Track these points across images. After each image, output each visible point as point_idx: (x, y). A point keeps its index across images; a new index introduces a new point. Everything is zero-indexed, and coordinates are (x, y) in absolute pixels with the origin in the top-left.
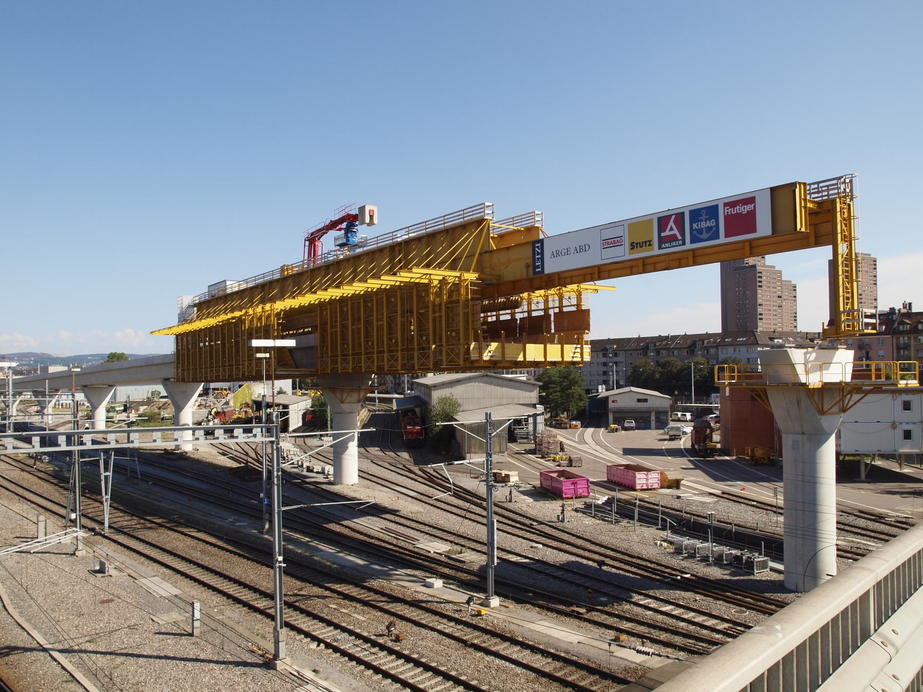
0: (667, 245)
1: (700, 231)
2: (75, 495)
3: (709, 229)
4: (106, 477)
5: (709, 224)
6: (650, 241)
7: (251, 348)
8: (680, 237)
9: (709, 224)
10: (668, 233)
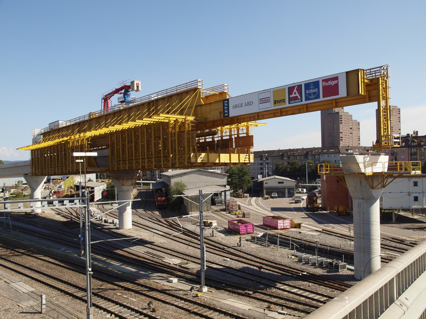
3: (314, 93)
5: (314, 91)
6: (284, 100)
8: (299, 98)
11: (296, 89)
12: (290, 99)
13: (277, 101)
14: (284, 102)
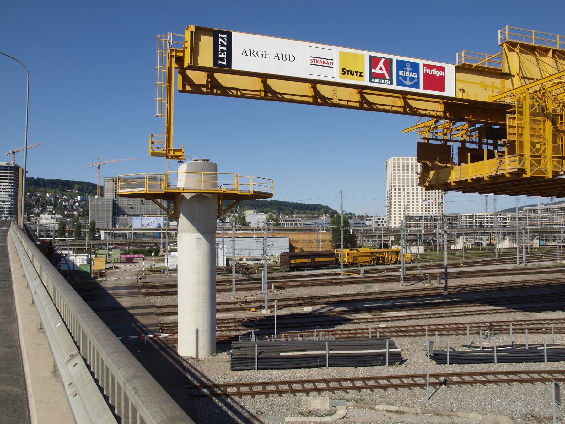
0: (377, 80)
1: (405, 78)
2: (321, 331)
3: (412, 79)
4: (366, 272)
5: (412, 75)
6: (361, 73)
7: (461, 50)
8: (388, 78)
9: (412, 75)
10: (377, 71)
11: (384, 74)
12: (372, 76)
13: (348, 71)
14: (360, 76)
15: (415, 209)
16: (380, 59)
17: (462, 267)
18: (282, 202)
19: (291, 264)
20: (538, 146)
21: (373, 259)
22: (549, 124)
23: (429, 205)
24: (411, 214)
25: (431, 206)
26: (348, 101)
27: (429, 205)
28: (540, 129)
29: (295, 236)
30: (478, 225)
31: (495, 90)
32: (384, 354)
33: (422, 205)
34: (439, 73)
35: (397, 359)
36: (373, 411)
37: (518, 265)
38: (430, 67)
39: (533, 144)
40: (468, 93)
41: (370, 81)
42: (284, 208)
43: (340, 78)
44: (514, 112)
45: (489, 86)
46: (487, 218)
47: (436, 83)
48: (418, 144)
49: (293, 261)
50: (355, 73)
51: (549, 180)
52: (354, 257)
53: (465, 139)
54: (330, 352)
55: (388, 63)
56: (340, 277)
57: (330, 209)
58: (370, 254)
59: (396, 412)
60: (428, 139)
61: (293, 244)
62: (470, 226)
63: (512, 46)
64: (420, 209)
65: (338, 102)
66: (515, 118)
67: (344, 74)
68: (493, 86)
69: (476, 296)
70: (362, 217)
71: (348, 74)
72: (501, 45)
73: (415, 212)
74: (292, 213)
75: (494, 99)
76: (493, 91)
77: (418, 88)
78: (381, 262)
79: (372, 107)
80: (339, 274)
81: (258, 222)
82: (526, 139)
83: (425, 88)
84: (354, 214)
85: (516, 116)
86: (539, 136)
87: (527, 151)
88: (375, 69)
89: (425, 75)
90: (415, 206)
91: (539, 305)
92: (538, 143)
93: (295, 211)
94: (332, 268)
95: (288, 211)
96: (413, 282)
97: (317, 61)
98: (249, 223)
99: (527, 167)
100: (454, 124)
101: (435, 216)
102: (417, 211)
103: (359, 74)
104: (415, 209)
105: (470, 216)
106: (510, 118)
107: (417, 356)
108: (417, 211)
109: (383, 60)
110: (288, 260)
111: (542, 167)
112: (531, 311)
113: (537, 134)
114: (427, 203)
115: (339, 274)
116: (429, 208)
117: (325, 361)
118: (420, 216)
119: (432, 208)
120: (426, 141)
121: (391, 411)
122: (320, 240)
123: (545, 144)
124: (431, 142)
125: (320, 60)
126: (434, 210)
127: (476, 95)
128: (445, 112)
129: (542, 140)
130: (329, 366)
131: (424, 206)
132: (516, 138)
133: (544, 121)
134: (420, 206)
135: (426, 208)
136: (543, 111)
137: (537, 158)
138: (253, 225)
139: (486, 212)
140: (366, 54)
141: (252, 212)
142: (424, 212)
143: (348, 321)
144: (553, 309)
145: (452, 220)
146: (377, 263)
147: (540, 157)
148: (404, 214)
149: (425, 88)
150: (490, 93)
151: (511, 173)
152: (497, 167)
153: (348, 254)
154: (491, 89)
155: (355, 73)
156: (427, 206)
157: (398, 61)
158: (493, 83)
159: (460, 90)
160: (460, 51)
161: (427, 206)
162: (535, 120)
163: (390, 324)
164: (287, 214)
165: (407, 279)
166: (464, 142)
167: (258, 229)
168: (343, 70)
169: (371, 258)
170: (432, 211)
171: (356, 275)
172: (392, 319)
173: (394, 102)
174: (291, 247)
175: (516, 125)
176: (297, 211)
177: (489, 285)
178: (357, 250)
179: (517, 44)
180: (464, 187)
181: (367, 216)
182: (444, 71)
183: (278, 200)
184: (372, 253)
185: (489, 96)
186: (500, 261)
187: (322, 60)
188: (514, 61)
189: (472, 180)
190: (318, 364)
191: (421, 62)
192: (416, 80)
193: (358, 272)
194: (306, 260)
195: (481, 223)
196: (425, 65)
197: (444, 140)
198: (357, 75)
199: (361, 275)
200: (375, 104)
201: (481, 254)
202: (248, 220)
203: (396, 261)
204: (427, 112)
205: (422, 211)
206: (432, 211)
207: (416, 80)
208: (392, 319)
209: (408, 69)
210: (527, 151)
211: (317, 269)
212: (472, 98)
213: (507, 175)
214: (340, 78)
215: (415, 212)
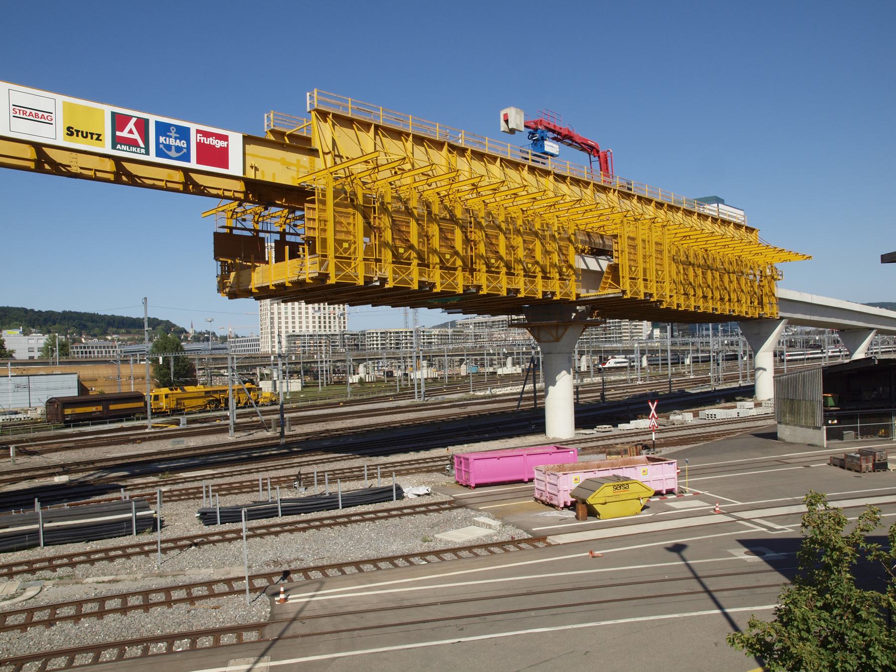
1: (169, 147)
3: (178, 149)
4: (190, 422)
6: (99, 135)
8: (142, 145)
9: (178, 143)
10: (125, 134)
11: (136, 140)
12: (116, 141)
13: (78, 131)
14: (98, 139)
15: (304, 325)
16: (129, 118)
17: (342, 406)
18: (85, 314)
19: (65, 416)
20: (346, 245)
21: (210, 402)
22: (360, 219)
23: (325, 318)
24: (297, 332)
25: (327, 320)
26: (96, 170)
27: (325, 318)
28: (349, 224)
29: (87, 372)
30: (395, 343)
31: (302, 170)
32: (129, 520)
33: (314, 318)
34: (220, 144)
35: (151, 524)
36: (79, 586)
37: (417, 401)
38: (207, 134)
39: (338, 242)
40: (263, 172)
41: (114, 147)
42: (89, 324)
43: (65, 140)
44: (313, 202)
45: (293, 165)
46: (406, 336)
47: (220, 157)
48: (216, 235)
49: (68, 411)
50: (89, 136)
51: (360, 288)
52: (177, 399)
53: (284, 230)
54: (46, 525)
55: (142, 125)
56: (147, 431)
57: (174, 326)
58: (203, 394)
59: (109, 582)
60: (231, 229)
61: (86, 384)
62: (383, 349)
63: (323, 115)
64: (311, 325)
65: (79, 171)
66: (314, 209)
67: (72, 134)
68: (299, 165)
69: (326, 443)
70: (224, 339)
71: (77, 136)
72: (310, 112)
73: (304, 329)
74: (105, 333)
75: (300, 181)
76: (298, 171)
77: (189, 161)
78: (223, 405)
79: (134, 181)
80: (146, 427)
81: (31, 350)
82: (330, 236)
83: (199, 162)
84: (214, 334)
85: (316, 206)
86: (348, 233)
87: (331, 252)
88: (122, 131)
89: (199, 145)
90: (304, 320)
91: (386, 449)
92: (346, 241)
93: (110, 329)
94: (138, 419)
95: (97, 330)
96: (252, 432)
97: (21, 112)
98: (13, 351)
99: (332, 271)
100: (266, 209)
101: (333, 335)
102: (307, 327)
103: (95, 137)
104: (304, 325)
105: (381, 333)
106: (309, 208)
107: (182, 519)
108: (307, 327)
109: (134, 120)
110: (59, 409)
111: (349, 271)
112: (377, 456)
113: (345, 230)
114: (317, 315)
115: (146, 427)
116: (325, 322)
117: (39, 539)
118: (311, 336)
119: (330, 322)
120: (227, 231)
121: (103, 582)
122: (135, 375)
123: (355, 243)
124: (235, 232)
125: (28, 111)
126: (332, 325)
127: (274, 175)
128: (246, 194)
129: (352, 238)
130: (45, 545)
131: (317, 320)
132: (316, 234)
133: (354, 214)
134: (311, 320)
135: (320, 322)
136: (352, 200)
137: (344, 260)
138: (21, 354)
139: (407, 327)
140: (108, 110)
141: (17, 332)
142: (317, 329)
143: (117, 488)
144: (406, 451)
145: (357, 343)
146: (217, 406)
147: (350, 259)
148: (287, 332)
149: (199, 162)
150: (294, 174)
151: (312, 278)
152: (298, 270)
153: (167, 396)
154: (295, 168)
155: (89, 136)
156: (322, 320)
157: (158, 124)
158: (298, 161)
159: (252, 167)
160: (268, 112)
161: (322, 320)
162: (341, 212)
163: (181, 486)
164: (95, 336)
165: (238, 428)
166: (283, 234)
167: (31, 362)
168: (69, 129)
169: (205, 401)
170: (330, 327)
171: (174, 427)
172: (186, 480)
173: (169, 175)
174: (82, 389)
175: (316, 217)
176: (114, 329)
177: (362, 427)
178: (183, 390)
179: (329, 113)
180: (283, 293)
181: (237, 337)
182: (227, 140)
183: (78, 311)
184: (207, 392)
185: (293, 177)
186: (397, 397)
187: (34, 112)
188: (323, 134)
189: (275, 285)
190: (27, 543)
191: (193, 127)
192: (185, 150)
193: (178, 424)
194: (94, 409)
195: (397, 344)
196: (198, 131)
197: (255, 230)
198: (92, 138)
199: (181, 426)
200: (139, 178)
201: (392, 387)
202: (8, 346)
203: (246, 403)
204: (220, 192)
205: (314, 327)
206: (330, 327)
207: (185, 150)
208: (186, 480)
209: (173, 134)
210: (331, 252)
211: (110, 422)
212: (268, 178)
213: (308, 281)
214: (65, 140)
215: (304, 329)
